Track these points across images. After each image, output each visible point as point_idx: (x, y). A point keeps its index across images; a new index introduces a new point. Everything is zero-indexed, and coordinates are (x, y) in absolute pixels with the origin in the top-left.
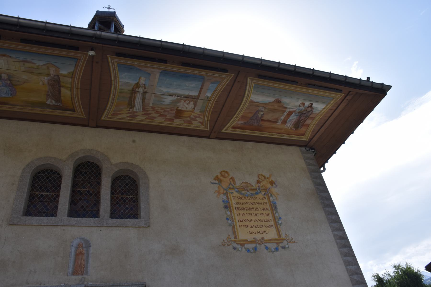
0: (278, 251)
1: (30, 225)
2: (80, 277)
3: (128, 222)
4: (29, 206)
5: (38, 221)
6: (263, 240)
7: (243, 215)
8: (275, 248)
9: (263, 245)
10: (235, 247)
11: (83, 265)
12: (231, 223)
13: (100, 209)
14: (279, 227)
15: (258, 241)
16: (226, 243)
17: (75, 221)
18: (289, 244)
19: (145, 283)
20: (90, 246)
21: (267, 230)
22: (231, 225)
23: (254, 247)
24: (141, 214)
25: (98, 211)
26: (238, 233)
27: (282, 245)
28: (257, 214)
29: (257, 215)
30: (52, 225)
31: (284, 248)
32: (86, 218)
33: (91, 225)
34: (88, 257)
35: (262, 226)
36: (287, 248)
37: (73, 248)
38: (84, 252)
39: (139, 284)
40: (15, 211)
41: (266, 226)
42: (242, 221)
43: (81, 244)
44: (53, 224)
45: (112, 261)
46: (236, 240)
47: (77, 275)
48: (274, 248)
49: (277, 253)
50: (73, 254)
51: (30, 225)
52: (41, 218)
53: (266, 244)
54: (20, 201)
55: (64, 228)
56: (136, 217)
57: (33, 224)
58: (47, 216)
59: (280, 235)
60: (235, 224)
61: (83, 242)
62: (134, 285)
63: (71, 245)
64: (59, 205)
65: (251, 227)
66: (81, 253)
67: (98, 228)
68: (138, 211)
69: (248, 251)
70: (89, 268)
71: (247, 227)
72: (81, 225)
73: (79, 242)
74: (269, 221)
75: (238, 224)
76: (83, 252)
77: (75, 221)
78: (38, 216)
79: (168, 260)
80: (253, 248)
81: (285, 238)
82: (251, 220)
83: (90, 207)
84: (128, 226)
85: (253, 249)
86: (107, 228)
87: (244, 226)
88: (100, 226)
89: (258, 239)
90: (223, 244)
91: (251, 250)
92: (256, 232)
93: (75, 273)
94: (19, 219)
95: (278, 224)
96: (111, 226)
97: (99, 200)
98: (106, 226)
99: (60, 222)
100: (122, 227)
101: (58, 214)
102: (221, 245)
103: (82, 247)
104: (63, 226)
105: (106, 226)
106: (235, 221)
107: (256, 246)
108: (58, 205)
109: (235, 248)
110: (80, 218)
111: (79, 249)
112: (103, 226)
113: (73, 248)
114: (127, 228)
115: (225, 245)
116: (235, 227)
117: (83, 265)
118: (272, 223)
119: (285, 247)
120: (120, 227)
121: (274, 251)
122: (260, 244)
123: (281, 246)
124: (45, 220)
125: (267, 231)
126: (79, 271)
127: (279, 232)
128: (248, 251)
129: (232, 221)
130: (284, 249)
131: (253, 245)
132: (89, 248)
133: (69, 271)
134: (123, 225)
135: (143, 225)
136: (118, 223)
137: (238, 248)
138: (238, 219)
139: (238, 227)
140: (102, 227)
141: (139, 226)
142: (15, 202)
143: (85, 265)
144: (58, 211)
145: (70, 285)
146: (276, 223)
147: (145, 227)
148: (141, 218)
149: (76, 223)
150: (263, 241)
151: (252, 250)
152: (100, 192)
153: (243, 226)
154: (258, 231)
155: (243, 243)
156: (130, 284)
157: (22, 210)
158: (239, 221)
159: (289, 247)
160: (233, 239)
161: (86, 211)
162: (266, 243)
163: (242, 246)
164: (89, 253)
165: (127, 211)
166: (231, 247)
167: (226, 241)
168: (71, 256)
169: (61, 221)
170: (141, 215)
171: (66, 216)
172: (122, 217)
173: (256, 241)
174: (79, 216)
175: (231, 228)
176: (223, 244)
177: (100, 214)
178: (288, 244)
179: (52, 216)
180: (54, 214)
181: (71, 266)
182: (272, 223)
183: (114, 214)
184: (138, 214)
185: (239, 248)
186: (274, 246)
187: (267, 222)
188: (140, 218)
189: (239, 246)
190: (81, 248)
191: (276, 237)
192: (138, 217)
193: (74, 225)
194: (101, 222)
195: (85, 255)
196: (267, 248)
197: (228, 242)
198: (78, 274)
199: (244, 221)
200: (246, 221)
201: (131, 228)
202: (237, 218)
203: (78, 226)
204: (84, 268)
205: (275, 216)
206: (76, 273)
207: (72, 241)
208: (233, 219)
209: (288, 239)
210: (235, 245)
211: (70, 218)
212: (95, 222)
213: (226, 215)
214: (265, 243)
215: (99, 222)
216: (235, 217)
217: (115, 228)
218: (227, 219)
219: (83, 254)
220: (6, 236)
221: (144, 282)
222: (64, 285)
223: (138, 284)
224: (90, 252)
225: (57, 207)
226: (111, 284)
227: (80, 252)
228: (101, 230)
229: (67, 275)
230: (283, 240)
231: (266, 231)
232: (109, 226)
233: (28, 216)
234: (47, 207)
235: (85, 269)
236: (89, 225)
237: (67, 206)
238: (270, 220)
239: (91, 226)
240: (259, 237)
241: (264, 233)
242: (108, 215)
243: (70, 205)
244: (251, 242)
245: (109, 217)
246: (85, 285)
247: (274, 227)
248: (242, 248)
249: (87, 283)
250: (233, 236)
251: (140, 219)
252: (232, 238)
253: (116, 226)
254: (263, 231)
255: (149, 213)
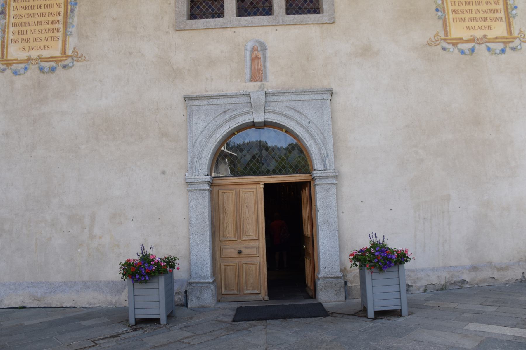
0: (505, 54)
1: (198, 29)
2: (259, 83)
3: (308, 18)
4: (192, 8)
5: (205, 24)
6: (484, 39)
7: (460, 4)
8: (500, 49)
9: (484, 45)
10: (444, 48)
11: (260, 71)
12: (442, 16)
13: (273, 5)
14: (511, 20)
15: (478, 40)
16: (433, 42)
17: (246, 21)
18: (523, 44)
19: (331, 90)
20: (266, 49)
21: (493, 24)
22: (442, 19)
23: (471, 47)
24: (323, 7)
25: (271, 7)
26: (450, 29)
27: (511, 45)
28: (481, 2)
29: (480, 3)
30: (221, 27)
31: (514, 49)
32: (257, 16)
33: (264, 24)
34: (265, 61)
35: (486, 19)
36: (519, 50)
37: (247, 52)
38: (260, 56)
39: (325, 91)
40: (179, 15)
41: (492, 19)
42: (457, 12)
43: (256, 47)
44: (222, 26)
45: (292, 65)
46: (447, 38)
47: (255, 82)
48: (499, 50)
49: (503, 56)
50: (248, 59)
51: (198, 29)
52: (208, 20)
53: (488, 44)
54: (182, 3)
55: (234, 30)
56: (318, 11)
57: (201, 28)
58: (213, 17)
59: (511, 31)
60: (447, 16)
61: (257, 44)
62: (319, 91)
63: (245, 48)
64: (225, 3)
65: (469, 20)
66: (257, 58)
67: (273, 27)
68: (319, 5)
69: (462, 52)
70: (267, 74)
71: (464, 20)
72: (254, 25)
73: (254, 45)
74: (497, 11)
75: (452, 16)
76: (259, 56)
77: (246, 21)
78: (204, 18)
79: (359, 63)
80: (470, 49)
81: (518, 35)
82: (470, 11)
83: (261, 3)
84: (308, 23)
85: (469, 50)
86: (283, 26)
87: (460, 19)
88: (275, 25)
89: (478, 37)
90: (428, 43)
91: (467, 51)
92: (477, 28)
93: (253, 79)
94: (184, 24)
95: (510, 15)
96: (287, 24)
97: (271, 6)
98: (281, 24)
99: (229, 23)
100: (302, 24)
101: (225, 14)
102: (426, 45)
103: (257, 50)
104: (232, 27)
105: (282, 24)
106: (448, 13)
107: (474, 46)
108: (224, 4)
109: (444, 49)
110: (251, 16)
111: (254, 53)
112: (279, 24)
113: (247, 52)
114: (307, 26)
115: (431, 45)
116: (447, 21)
117: (260, 71)
118: (502, 15)
119: (515, 48)
120: (299, 24)
121: (499, 54)
122: (480, 43)
123: (509, 47)
124: (212, 22)
125: (492, 26)
126: (258, 77)
127: (510, 27)
128: (462, 52)
129: (444, 13)
130: (514, 50)
131: (470, 45)
132: (266, 51)
133: (246, 77)
134: (302, 22)
135: (326, 22)
136: (296, 21)
137: (449, 48)
138: (452, 10)
139: (451, 20)
140: (278, 25)
141: (322, 23)
142: (176, 4)
143: (263, 71)
144: (225, 11)
145: (250, 92)
146: (508, 15)
147: (329, 23)
148: (323, 12)
149: (247, 23)
150: (485, 40)
151: (468, 52)
152: (272, 1)
153: (458, 20)
154: (479, 27)
155: (455, 42)
156: (315, 90)
157: (186, 13)
158: (454, 13)
159: (521, 49)
160: (443, 37)
161: (256, 8)
162: (489, 42)
163: (455, 46)
164: (266, 57)
165: (305, 5)
166: (439, 47)
167: (433, 39)
168: (247, 61)
169: (231, 22)
170: (323, 8)
171: (235, 15)
172: (300, 13)
173: (475, 39)
174: (249, 15)
175: (441, 22)
176: (428, 43)
177: (274, 10)
178: (520, 44)
179: (219, 16)
180: (220, 14)
181: (248, 72)
182: (504, 22)
183: (290, 9)
184: (320, 7)
185: (450, 49)
186: (501, 46)
187: (494, 12)
188: (323, 13)
189: (450, 46)
190: (256, 52)
191: (505, 34)
192: (319, 11)
193: (245, 26)
194: (276, 20)
195: (262, 59)
196: (489, 49)
197: (436, 40)
198: (257, 81)
199: (460, 12)
200: (463, 13)
201: (312, 26)
202: (451, 8)
203: (250, 27)
204: (262, 74)
205: (508, 4)
206: (254, 79)
207: (245, 44)
208: (445, 10)
209: (522, 36)
210: (445, 45)
211: (239, 18)
212: (269, 21)
213: (436, 4)
214: (487, 42)
215: (274, 20)
216: (447, 6)
217: (293, 26)
218: (437, 10)
219: (259, 58)
220: (175, 43)
221: (331, 88)
222: (243, 92)
223: (323, 90)
224: (266, 56)
225: (222, 6)
226: (294, 90)
227: (255, 56)
228: (276, 30)
229: (245, 82)
230: (515, 38)
231: (491, 26)
232: (285, 24)
233: (193, 19)
234: (212, 8)
235: (263, 75)
236: (262, 25)
237: (234, 3)
238: (499, 11)
239: (265, 25)
240: (479, 34)
241: (488, 29)
242: (283, 10)
243: (237, 2)
244: (468, 41)
245: (285, 13)
246: (265, 92)
247: (504, 20)
248: (454, 48)
249: (268, 90)
250: (443, 32)
251: (322, 13)
252: (442, 35)
253: (294, 24)
254: (486, 27)
255: (333, 5)
